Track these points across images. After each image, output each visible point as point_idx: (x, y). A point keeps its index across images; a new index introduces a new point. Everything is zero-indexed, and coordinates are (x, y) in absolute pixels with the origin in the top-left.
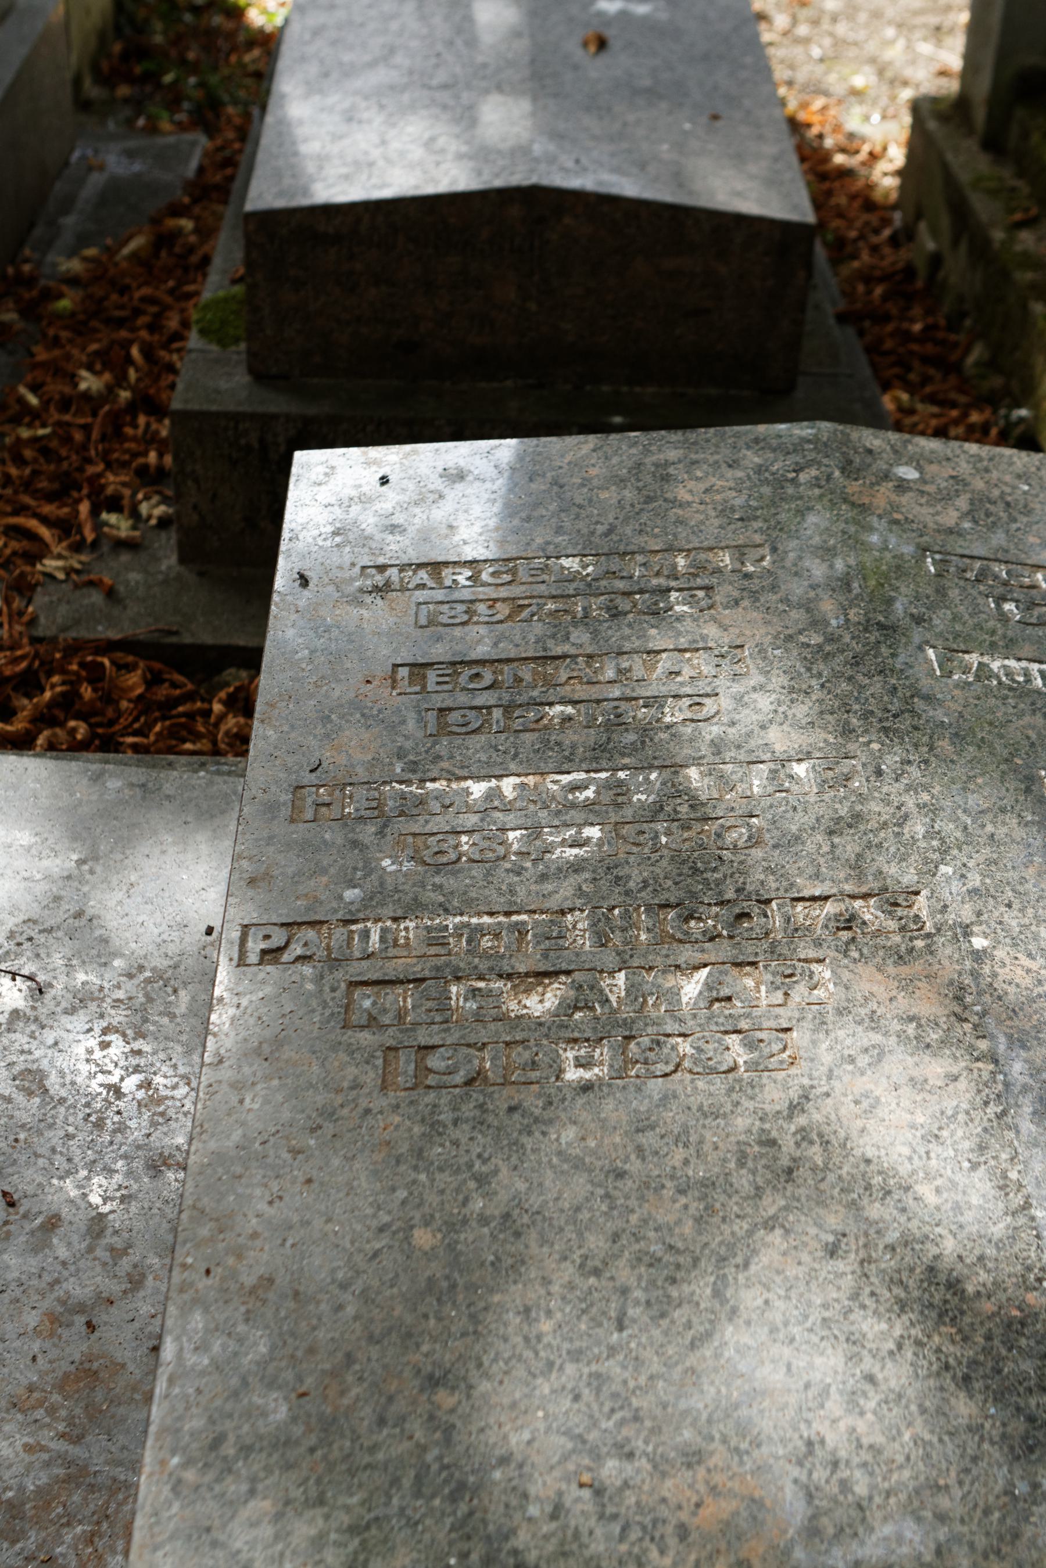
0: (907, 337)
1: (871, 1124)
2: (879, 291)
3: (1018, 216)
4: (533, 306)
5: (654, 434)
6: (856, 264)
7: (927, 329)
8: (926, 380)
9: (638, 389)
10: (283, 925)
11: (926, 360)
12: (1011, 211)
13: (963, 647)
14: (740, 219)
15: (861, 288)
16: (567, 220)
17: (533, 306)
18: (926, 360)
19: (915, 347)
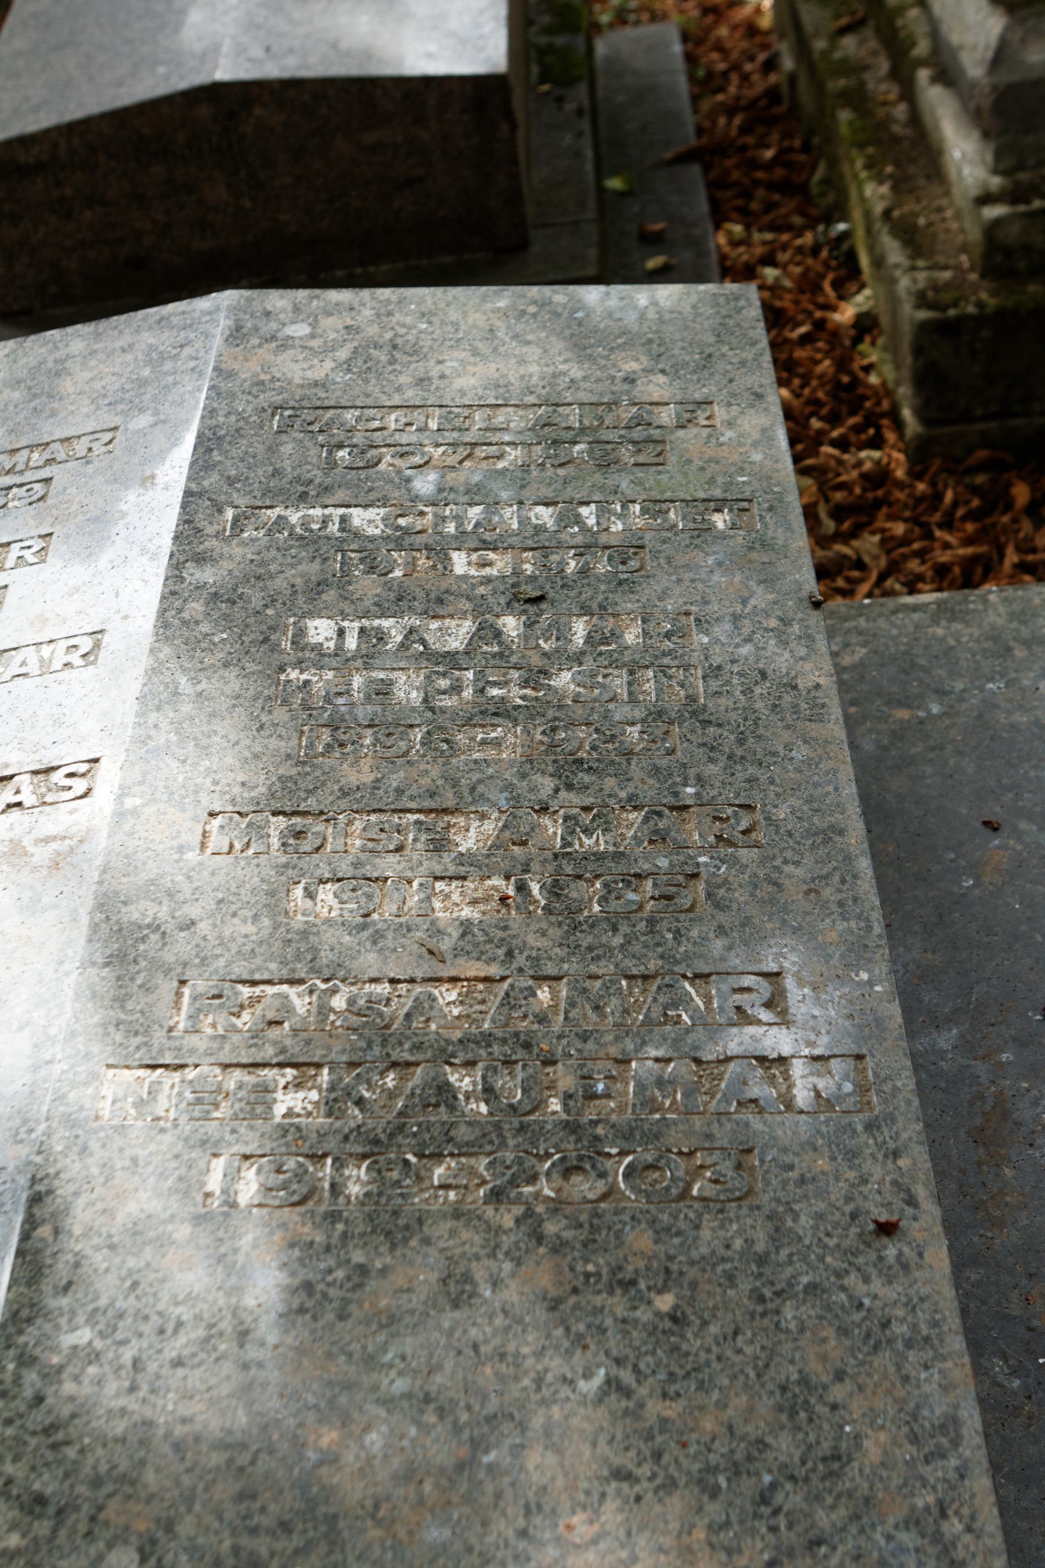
0: (755, 164)
1: (573, 885)
2: (738, 120)
3: (844, 21)
4: (247, 203)
5: (69, 330)
6: (720, 97)
7: (782, 152)
8: (769, 206)
9: (372, 269)
10: (35, 773)
11: (771, 186)
12: (838, 16)
13: (268, 503)
14: (428, 82)
15: (722, 121)
16: (258, 111)
17: (247, 203)
18: (771, 186)
19: (760, 175)
